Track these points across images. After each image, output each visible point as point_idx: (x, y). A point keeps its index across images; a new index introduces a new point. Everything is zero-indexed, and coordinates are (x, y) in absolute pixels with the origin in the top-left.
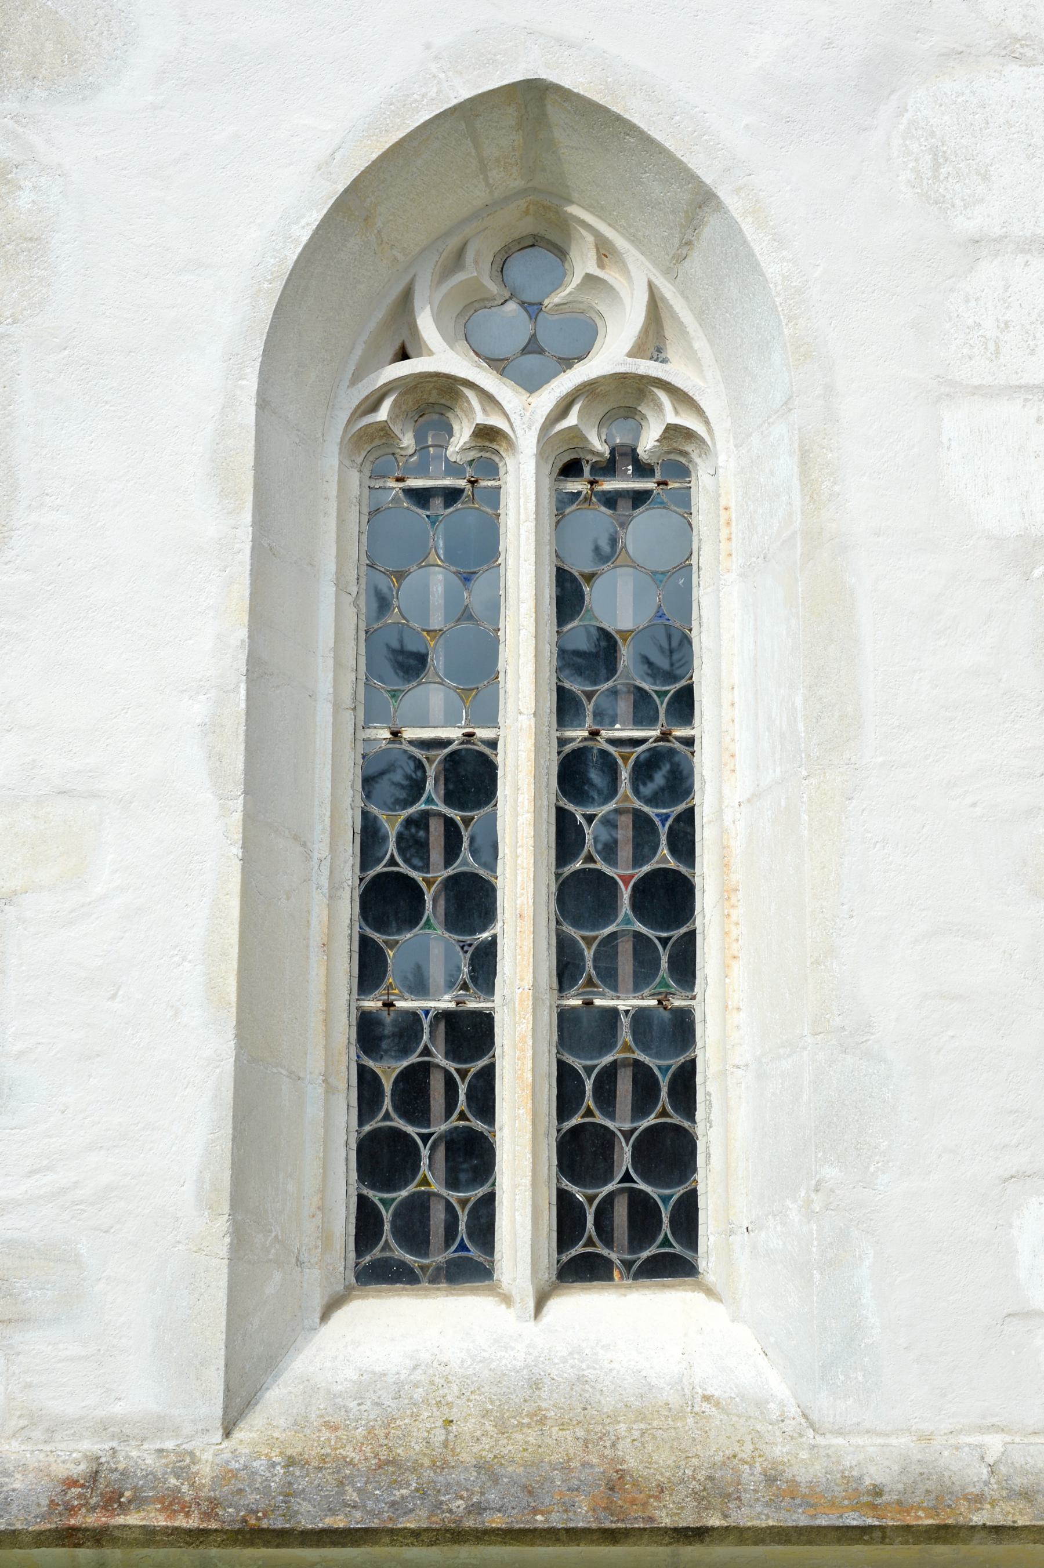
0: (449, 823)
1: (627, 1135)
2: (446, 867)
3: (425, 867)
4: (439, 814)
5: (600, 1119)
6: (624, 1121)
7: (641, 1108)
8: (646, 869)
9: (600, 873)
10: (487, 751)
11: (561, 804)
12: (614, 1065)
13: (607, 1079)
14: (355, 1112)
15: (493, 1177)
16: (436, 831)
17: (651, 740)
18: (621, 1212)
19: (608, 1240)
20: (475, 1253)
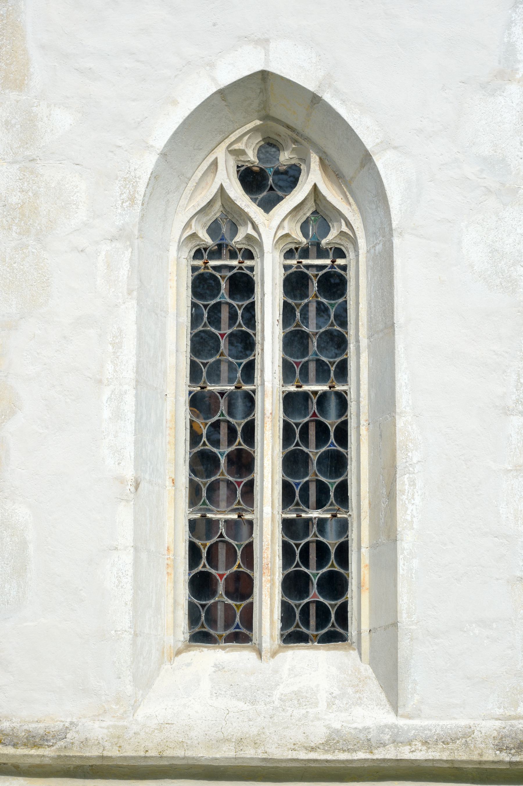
0: (231, 306)
1: (315, 575)
2: (229, 329)
3: (219, 329)
4: (227, 303)
5: (303, 569)
6: (313, 570)
7: (320, 565)
8: (325, 570)
9: (302, 451)
10: (248, 272)
11: (285, 419)
12: (308, 604)
13: (305, 429)
14: (188, 443)
15: (254, 413)
16: (224, 430)
17: (328, 267)
18: (312, 367)
19: (307, 624)
20: (244, 630)
